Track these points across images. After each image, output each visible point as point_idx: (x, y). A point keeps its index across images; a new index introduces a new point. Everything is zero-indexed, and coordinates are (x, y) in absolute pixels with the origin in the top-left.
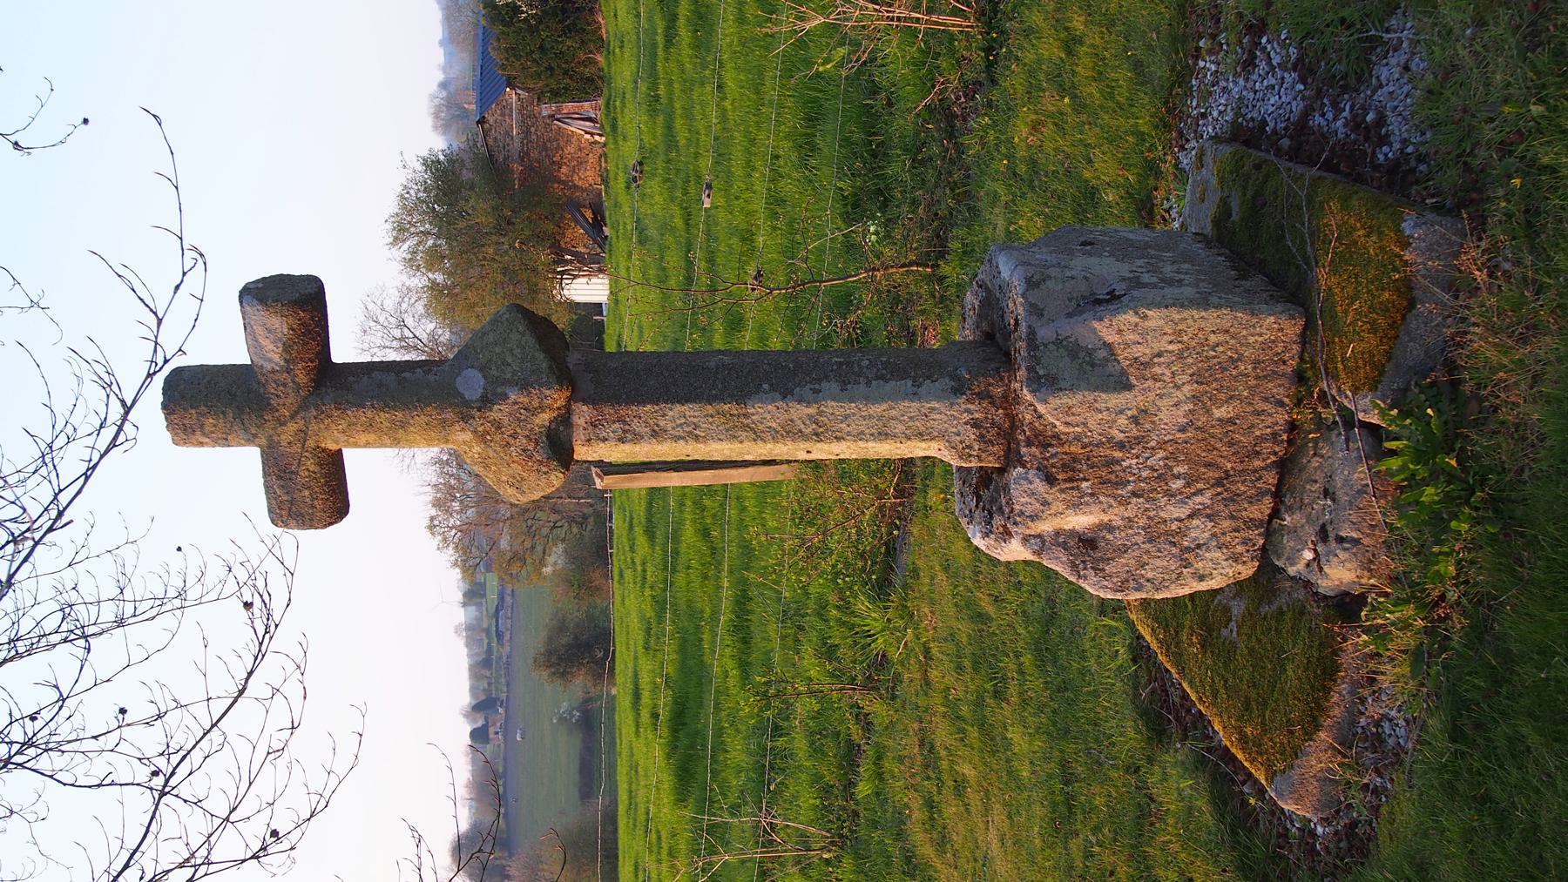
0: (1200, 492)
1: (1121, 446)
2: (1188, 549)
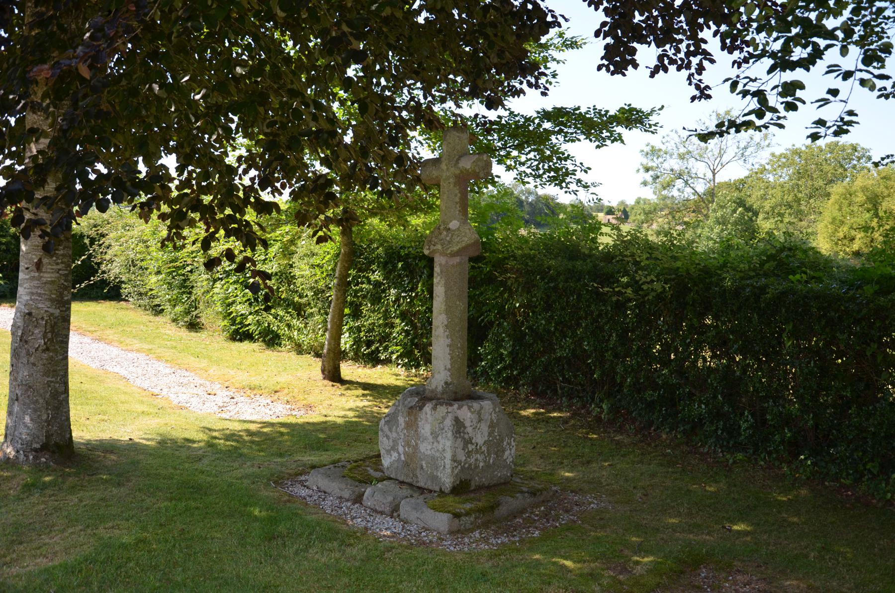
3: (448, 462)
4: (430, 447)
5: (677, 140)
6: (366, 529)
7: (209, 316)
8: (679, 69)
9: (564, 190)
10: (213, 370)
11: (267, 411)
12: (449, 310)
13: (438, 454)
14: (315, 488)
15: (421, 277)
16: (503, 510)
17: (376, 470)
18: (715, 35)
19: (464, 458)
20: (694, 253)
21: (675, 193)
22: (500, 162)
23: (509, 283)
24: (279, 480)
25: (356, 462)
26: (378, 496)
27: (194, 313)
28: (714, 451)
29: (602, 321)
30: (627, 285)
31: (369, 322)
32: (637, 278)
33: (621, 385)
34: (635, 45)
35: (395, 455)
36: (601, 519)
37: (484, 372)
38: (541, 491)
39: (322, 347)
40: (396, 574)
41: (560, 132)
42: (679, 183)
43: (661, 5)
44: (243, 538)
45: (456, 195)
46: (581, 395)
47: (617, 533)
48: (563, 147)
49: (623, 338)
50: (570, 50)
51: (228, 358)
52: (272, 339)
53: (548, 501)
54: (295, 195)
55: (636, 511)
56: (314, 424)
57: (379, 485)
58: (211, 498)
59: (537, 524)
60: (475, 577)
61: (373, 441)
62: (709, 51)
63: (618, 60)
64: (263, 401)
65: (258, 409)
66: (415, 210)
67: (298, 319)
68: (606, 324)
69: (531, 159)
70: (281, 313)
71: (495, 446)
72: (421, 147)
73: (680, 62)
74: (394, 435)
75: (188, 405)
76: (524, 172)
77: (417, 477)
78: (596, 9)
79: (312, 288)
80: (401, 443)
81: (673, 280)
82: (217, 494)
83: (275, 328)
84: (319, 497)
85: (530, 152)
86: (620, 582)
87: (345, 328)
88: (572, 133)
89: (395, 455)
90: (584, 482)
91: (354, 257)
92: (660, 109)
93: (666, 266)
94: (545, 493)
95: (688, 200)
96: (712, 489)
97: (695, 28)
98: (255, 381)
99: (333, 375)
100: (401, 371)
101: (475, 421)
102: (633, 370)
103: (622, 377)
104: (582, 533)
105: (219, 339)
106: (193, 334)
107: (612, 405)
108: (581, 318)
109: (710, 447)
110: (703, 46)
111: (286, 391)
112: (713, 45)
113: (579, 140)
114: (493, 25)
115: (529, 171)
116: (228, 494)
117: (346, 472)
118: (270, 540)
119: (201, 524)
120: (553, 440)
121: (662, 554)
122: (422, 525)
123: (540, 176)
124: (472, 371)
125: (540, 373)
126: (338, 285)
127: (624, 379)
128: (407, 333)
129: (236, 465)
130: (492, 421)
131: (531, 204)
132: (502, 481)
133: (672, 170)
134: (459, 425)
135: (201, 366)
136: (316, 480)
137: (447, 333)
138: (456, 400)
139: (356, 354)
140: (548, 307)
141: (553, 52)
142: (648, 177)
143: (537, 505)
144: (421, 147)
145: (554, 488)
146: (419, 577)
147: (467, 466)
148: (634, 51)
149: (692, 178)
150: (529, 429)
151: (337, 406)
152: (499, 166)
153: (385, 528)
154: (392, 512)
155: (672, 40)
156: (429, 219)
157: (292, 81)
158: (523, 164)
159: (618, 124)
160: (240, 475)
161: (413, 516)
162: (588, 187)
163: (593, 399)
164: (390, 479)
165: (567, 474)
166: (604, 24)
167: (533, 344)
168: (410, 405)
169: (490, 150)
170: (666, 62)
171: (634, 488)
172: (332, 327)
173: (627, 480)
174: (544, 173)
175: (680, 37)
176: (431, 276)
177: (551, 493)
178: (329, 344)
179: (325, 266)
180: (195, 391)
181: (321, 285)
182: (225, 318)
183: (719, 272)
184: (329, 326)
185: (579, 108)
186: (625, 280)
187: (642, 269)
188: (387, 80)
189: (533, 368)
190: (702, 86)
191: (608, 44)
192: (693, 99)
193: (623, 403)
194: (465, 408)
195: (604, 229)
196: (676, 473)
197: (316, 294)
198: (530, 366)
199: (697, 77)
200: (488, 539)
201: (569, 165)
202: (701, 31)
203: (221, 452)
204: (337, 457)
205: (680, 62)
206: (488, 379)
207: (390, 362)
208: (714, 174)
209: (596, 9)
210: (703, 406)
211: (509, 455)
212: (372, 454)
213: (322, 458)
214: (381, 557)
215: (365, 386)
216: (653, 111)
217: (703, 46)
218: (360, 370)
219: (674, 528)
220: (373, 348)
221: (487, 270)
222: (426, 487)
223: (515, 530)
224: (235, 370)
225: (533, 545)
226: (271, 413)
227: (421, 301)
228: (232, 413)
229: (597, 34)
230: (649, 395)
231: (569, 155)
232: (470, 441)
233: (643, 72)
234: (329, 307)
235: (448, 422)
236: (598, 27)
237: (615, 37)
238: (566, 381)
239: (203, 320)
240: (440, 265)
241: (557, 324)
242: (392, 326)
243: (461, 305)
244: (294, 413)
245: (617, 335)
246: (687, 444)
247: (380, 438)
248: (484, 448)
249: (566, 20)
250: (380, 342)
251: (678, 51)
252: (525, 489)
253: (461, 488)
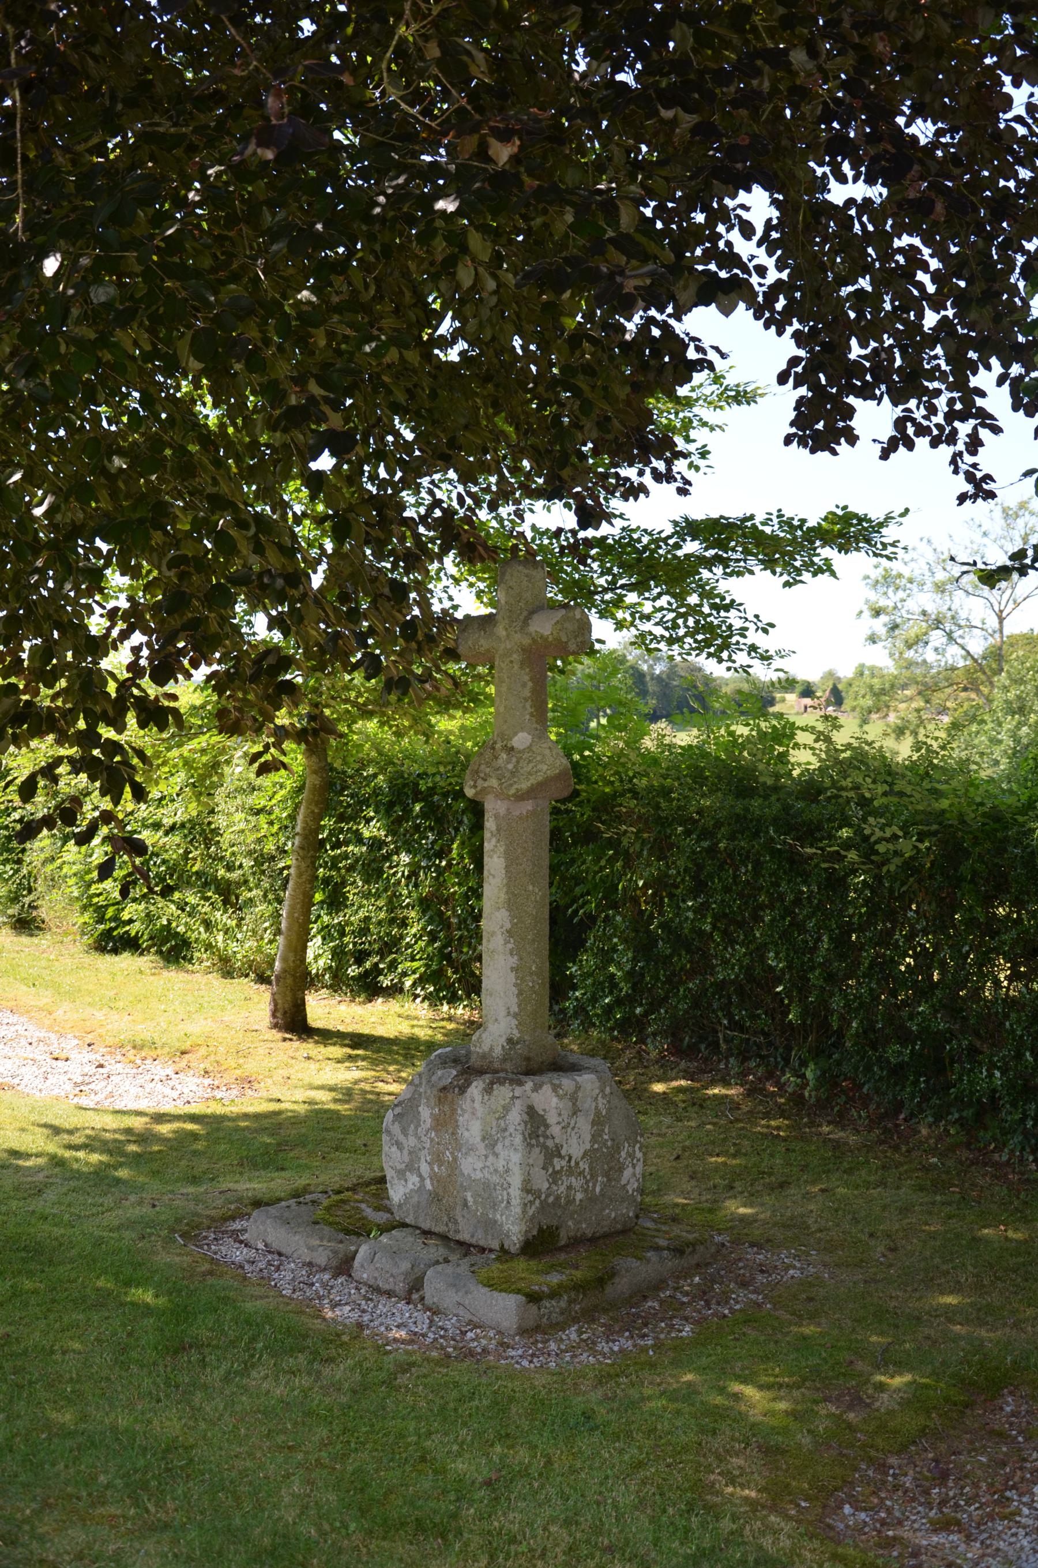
3: (516, 1192)
4: (479, 1165)
5: (931, 557)
6: (360, 1326)
7: (54, 904)
8: (935, 443)
9: (725, 665)
10: (63, 1011)
11: (167, 1091)
12: (512, 904)
13: (495, 1179)
14: (261, 1246)
15: (457, 830)
16: (621, 1285)
17: (377, 1209)
18: (1000, 382)
19: (546, 1185)
20: (972, 784)
21: (930, 656)
22: (602, 614)
23: (625, 842)
24: (190, 1230)
25: (339, 1192)
26: (382, 1261)
27: (27, 900)
28: (1021, 1160)
29: (801, 913)
30: (847, 845)
31: (361, 914)
32: (867, 832)
33: (840, 1034)
34: (851, 400)
35: (413, 1179)
36: (810, 1299)
37: (581, 1010)
38: (693, 1245)
39: (271, 964)
40: (418, 1418)
41: (717, 560)
42: (937, 638)
44: (124, 1350)
45: (524, 685)
46: (764, 1053)
47: (841, 1328)
48: (723, 586)
49: (840, 942)
50: (735, 406)
51: (91, 987)
52: (174, 950)
53: (708, 1265)
54: (218, 683)
55: (876, 1281)
56: (257, 1116)
57: (384, 1239)
58: (61, 1269)
59: (688, 1311)
60: (572, 1422)
61: (371, 1149)
62: (990, 410)
63: (820, 426)
64: (160, 1070)
65: (149, 1086)
66: (446, 706)
67: (225, 911)
68: (809, 917)
69: (662, 609)
70: (192, 899)
71: (605, 1160)
72: (457, 592)
73: (935, 432)
74: (412, 1141)
75: (16, 1081)
76: (650, 633)
77: (456, 1222)
78: (780, 333)
79: (250, 853)
80: (425, 1156)
81: (935, 834)
82: (72, 1261)
83: (181, 929)
84: (269, 1263)
85: (660, 595)
86: (850, 1426)
87: (315, 928)
88: (738, 561)
89: (413, 1179)
90: (775, 1224)
91: (331, 792)
92: (902, 515)
93: (920, 807)
94: (701, 1248)
95: (953, 669)
96: (1018, 1236)
97: (962, 369)
98: (144, 1031)
99: (293, 1022)
100: (421, 1009)
101: (565, 1114)
102: (861, 1005)
103: (842, 1018)
104: (774, 1329)
105: (73, 950)
106: (25, 940)
107: (824, 1073)
108: (762, 907)
109: (1012, 1151)
110: (979, 402)
111: (203, 1051)
112: (997, 400)
113: (751, 572)
114: (589, 370)
115: (659, 631)
116: (94, 1261)
117: (320, 1213)
118: (176, 1353)
119: (42, 1324)
120: (713, 1143)
121: (930, 1368)
122: (468, 1316)
123: (679, 640)
124: (556, 1008)
125: (686, 1012)
126: (302, 848)
127: (845, 1022)
128: (433, 937)
129: (109, 1201)
130: (598, 1113)
131: (659, 679)
132: (619, 1227)
133: (924, 613)
134: (535, 1122)
135: (40, 1004)
136: (263, 1229)
137: (510, 946)
138: (529, 1072)
139: (335, 976)
140: (699, 887)
141: (700, 411)
142: (879, 625)
143: (686, 1274)
144: (457, 592)
145: (718, 1239)
146: (465, 1424)
147: (551, 1199)
148: (849, 412)
149: (960, 627)
150: (667, 1120)
151: (302, 1079)
152: (603, 621)
153: (397, 1324)
154: (410, 1292)
155: (921, 392)
156: (471, 720)
157: (214, 479)
158: (648, 618)
159: (826, 543)
160: (116, 1223)
161: (449, 1299)
162: (770, 658)
163: (787, 1060)
164: (405, 1225)
165: (742, 1210)
166: (794, 361)
167: (671, 956)
168: (442, 1084)
169: (582, 592)
170: (910, 430)
171: (871, 1235)
172: (289, 929)
173: (856, 1221)
174: (686, 635)
175: (936, 385)
176: (478, 826)
177: (713, 1250)
178: (284, 960)
179: (277, 810)
180: (29, 1052)
181: (270, 847)
182: (84, 908)
183: (1020, 819)
184: (283, 926)
185: (752, 517)
186: (845, 833)
187: (876, 813)
188: (391, 472)
189: (673, 1001)
190: (979, 475)
191: (802, 397)
192: (962, 498)
193: (845, 1068)
194: (547, 1089)
195: (801, 737)
196: (949, 1204)
197: (258, 863)
198: (666, 999)
199: (968, 459)
200: (594, 1343)
201: (734, 618)
202: (974, 374)
203: (78, 1175)
204: (301, 1182)
205: (935, 432)
206: (588, 1024)
207: (401, 990)
208: (1001, 620)
209: (780, 333)
210: (998, 1074)
211: (630, 1177)
212: (369, 1175)
213: (272, 1185)
214: (389, 1383)
215: (358, 1041)
216: (888, 518)
217: (979, 402)
218: (343, 1007)
219: (950, 1314)
220: (368, 965)
221: (585, 819)
222: (474, 1241)
223: (646, 1325)
224: (106, 1010)
225: (680, 1354)
226: (175, 1094)
227: (457, 875)
228: (100, 1097)
229: (782, 379)
230: (895, 1052)
231: (733, 601)
232: (556, 1152)
233: (867, 450)
234: (284, 887)
235: (516, 1116)
236: (784, 366)
237: (815, 386)
238: (735, 1025)
239: (43, 913)
240: (496, 816)
241: (716, 919)
242: (404, 924)
243: (538, 895)
244: (219, 1095)
245: (830, 938)
246: (968, 1145)
247: (385, 1148)
248: (584, 1166)
249: (723, 356)
250: (382, 953)
251: (932, 410)
252: (663, 1243)
253: (540, 1244)
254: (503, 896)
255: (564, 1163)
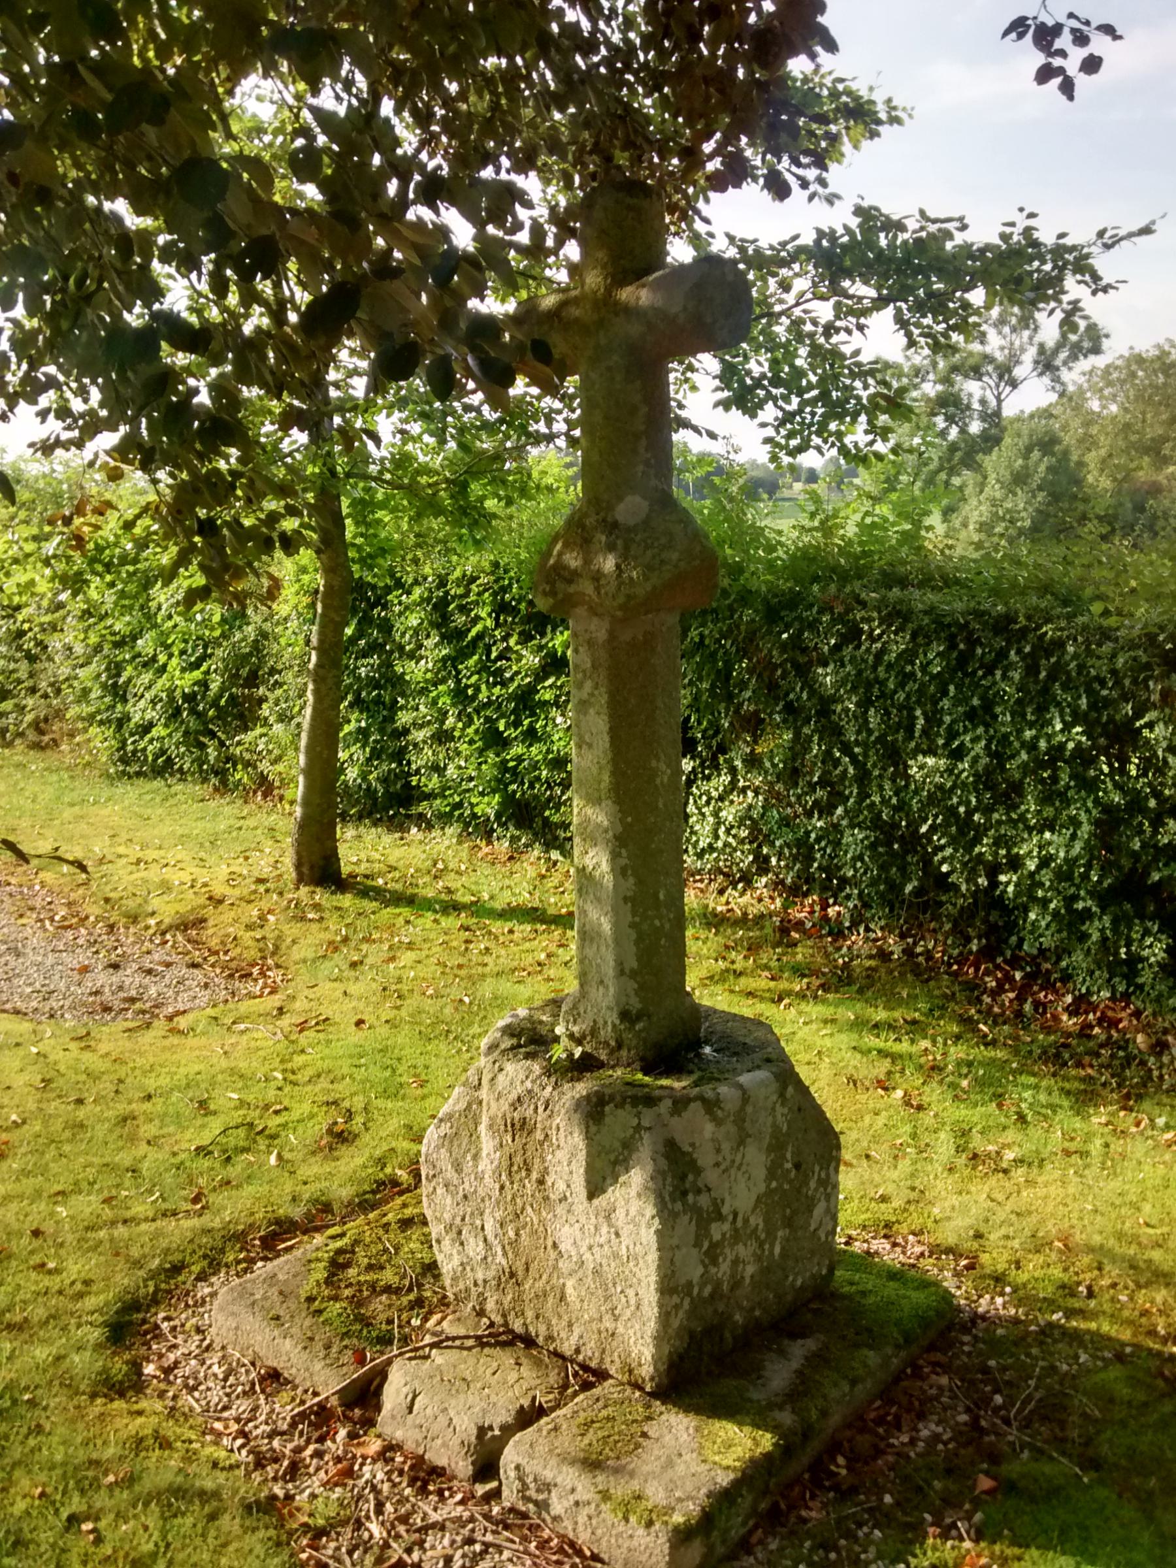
0: (505, 1254)
1: (541, 1182)
2: (460, 1233)
43: (741, 73)
113: (731, 238)
147: (708, 1290)
248: (756, 1221)
254: (606, 778)
255: (726, 1227)
